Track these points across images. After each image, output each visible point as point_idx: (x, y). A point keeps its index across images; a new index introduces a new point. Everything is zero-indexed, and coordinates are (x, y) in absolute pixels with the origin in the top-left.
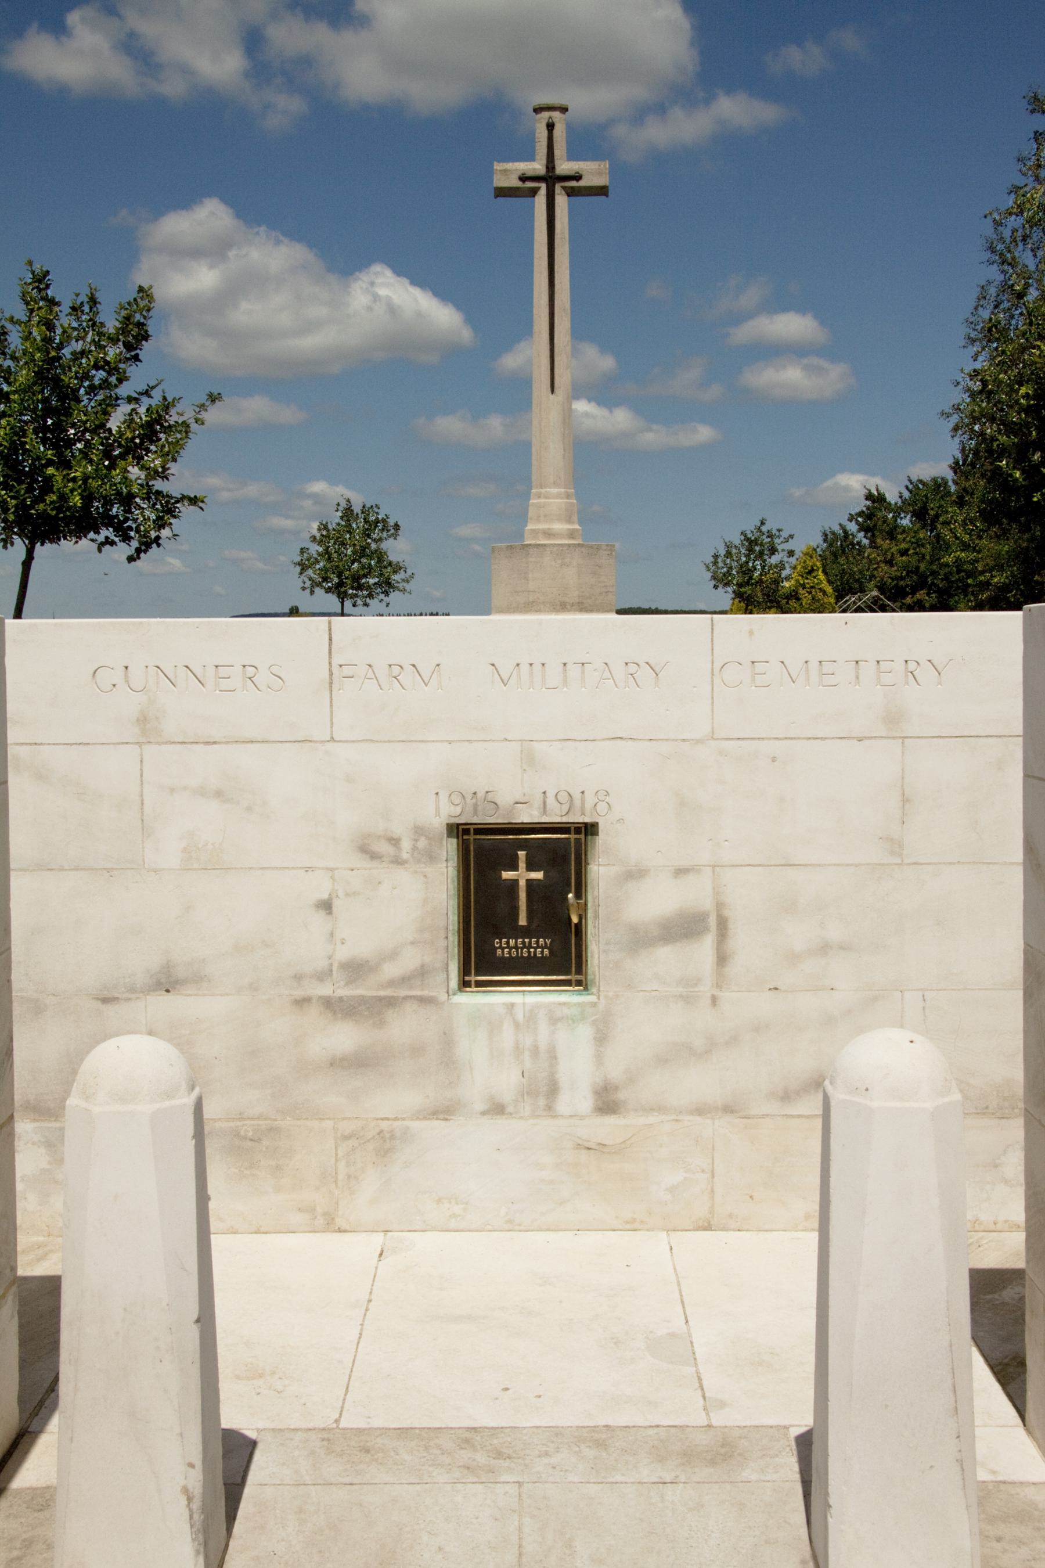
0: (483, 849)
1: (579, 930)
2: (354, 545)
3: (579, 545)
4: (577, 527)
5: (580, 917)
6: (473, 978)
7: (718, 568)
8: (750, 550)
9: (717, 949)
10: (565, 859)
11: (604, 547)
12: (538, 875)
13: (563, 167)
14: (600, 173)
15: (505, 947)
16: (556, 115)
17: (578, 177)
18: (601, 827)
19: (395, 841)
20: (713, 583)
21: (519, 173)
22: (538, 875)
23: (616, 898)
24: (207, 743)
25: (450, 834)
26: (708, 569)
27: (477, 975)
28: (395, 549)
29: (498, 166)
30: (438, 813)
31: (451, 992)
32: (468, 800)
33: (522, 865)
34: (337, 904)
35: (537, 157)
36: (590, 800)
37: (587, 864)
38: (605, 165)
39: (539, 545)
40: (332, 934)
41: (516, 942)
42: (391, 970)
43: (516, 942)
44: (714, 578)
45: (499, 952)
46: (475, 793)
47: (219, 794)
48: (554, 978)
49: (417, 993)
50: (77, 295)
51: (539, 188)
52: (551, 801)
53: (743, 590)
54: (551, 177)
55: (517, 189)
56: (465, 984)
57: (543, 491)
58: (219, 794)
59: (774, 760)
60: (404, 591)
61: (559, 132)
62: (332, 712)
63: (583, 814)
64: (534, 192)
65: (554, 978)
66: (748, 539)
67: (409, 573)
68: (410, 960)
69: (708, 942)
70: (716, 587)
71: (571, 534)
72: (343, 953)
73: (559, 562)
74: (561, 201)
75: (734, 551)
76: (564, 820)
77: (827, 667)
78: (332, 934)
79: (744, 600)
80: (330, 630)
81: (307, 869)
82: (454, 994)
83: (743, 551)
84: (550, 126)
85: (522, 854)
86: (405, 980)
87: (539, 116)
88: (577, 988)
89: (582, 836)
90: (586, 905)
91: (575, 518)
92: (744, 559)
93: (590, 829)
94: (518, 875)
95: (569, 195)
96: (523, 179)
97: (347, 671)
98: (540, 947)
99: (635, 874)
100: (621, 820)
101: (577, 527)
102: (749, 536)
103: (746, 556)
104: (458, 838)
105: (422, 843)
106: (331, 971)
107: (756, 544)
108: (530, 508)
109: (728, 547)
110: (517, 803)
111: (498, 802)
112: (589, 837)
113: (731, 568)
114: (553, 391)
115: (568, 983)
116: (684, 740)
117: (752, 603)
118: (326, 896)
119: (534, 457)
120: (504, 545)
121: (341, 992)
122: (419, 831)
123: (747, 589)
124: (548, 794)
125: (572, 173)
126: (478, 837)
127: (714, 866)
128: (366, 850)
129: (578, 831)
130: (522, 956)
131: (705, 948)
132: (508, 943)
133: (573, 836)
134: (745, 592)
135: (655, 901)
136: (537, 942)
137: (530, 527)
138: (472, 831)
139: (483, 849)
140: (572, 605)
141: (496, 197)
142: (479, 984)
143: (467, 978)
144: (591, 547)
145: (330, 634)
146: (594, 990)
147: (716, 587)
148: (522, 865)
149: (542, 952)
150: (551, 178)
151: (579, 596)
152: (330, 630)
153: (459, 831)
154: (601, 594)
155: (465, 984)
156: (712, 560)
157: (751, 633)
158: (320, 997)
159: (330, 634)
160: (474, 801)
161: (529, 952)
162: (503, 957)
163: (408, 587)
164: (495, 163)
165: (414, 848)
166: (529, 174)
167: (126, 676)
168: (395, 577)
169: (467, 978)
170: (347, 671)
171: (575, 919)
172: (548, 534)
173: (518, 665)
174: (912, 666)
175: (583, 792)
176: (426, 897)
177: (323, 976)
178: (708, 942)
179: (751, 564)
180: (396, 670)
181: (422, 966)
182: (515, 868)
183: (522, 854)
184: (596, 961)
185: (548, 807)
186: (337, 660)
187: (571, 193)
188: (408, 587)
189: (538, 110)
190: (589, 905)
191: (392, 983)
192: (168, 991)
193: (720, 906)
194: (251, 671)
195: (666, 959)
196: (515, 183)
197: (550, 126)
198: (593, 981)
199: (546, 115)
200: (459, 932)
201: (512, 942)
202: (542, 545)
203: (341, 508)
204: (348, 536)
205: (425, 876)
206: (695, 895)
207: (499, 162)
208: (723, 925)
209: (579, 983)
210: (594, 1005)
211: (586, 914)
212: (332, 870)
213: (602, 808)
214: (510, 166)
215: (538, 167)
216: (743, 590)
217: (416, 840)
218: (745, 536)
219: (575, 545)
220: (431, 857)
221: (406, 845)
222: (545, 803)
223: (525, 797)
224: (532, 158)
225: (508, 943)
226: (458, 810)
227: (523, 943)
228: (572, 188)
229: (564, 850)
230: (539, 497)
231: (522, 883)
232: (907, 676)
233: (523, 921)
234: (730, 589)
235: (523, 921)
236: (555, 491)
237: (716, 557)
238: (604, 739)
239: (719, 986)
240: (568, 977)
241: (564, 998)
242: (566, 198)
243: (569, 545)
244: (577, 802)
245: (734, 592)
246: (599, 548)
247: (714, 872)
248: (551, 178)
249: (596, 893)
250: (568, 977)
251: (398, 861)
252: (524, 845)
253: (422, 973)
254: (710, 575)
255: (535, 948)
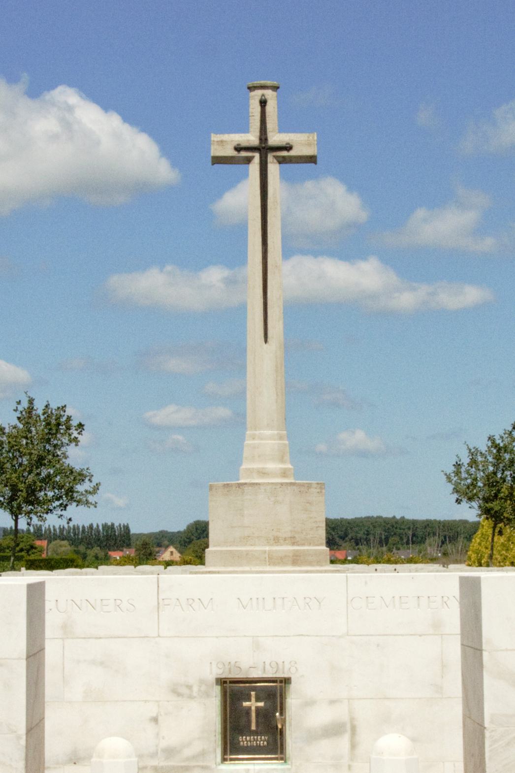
0: (233, 691)
1: (282, 732)
2: (30, 454)
3: (291, 484)
4: (290, 466)
5: (282, 726)
6: (228, 757)
7: (461, 479)
8: (498, 458)
9: (351, 741)
10: (274, 695)
11: (315, 486)
12: (261, 704)
13: (275, 138)
14: (309, 145)
15: (244, 740)
16: (269, 94)
17: (288, 148)
18: (292, 679)
19: (190, 687)
20: (456, 496)
21: (235, 144)
22: (261, 704)
23: (300, 716)
24: (96, 638)
25: (217, 684)
26: (449, 479)
27: (230, 755)
28: (75, 456)
29: (215, 138)
30: (211, 673)
31: (217, 764)
32: (226, 666)
33: (253, 699)
34: (160, 718)
35: (251, 129)
36: (287, 666)
37: (286, 698)
38: (314, 137)
39: (253, 484)
40: (158, 734)
41: (250, 738)
42: (188, 752)
43: (250, 738)
44: (456, 490)
45: (242, 743)
46: (230, 663)
47: (102, 663)
48: (269, 756)
49: (201, 764)
50: (19, 403)
51: (253, 157)
52: (268, 667)
53: (489, 505)
54: (264, 148)
55: (232, 157)
56: (224, 760)
57: (257, 432)
58: (102, 663)
59: (378, 645)
60: (87, 503)
61: (272, 108)
62: (159, 622)
63: (283, 673)
64: (249, 160)
65: (269, 756)
66: (496, 446)
67: (95, 480)
68: (197, 747)
69: (346, 737)
70: (458, 501)
71: (284, 473)
72: (163, 744)
73: (273, 499)
74: (273, 168)
75: (480, 459)
76: (274, 676)
77: (105, 602)
78: (158, 734)
79: (492, 516)
80: (158, 581)
81: (146, 701)
82: (219, 765)
83: (490, 459)
84: (263, 103)
85: (253, 693)
86: (194, 757)
87: (253, 94)
88: (281, 761)
89: (283, 684)
90: (285, 719)
91: (287, 457)
92: (491, 469)
93: (287, 681)
94: (252, 704)
95: (280, 163)
96: (238, 149)
97: (166, 602)
98: (262, 741)
99: (309, 703)
100: (303, 676)
101: (290, 466)
102: (498, 441)
103: (494, 465)
104: (221, 685)
105: (203, 688)
106: (157, 753)
107: (505, 451)
108: (245, 449)
109: (473, 453)
110: (250, 667)
111: (241, 667)
112: (287, 685)
113: (476, 479)
114: (266, 341)
115: (276, 759)
116: (333, 636)
117: (501, 521)
118: (155, 715)
119: (248, 402)
120: (221, 483)
121: (162, 764)
122: (202, 682)
123: (495, 505)
124: (266, 663)
125: (284, 144)
126: (231, 685)
127: (349, 699)
128: (175, 691)
129: (281, 682)
130: (253, 746)
131: (344, 741)
132: (246, 739)
133: (278, 684)
134: (492, 509)
135: (320, 716)
136: (261, 738)
137: (244, 466)
138: (228, 682)
139: (233, 691)
140: (285, 539)
141: (213, 164)
142: (231, 760)
143: (225, 757)
144: (303, 485)
145: (158, 584)
146: (289, 762)
147: (458, 501)
148: (253, 699)
149: (263, 743)
150: (264, 149)
151: (291, 531)
152: (158, 581)
153: (222, 682)
154: (312, 529)
155: (224, 760)
156: (453, 469)
157: (366, 583)
158: (152, 766)
159: (158, 584)
160: (229, 666)
161: (257, 744)
162: (243, 746)
163: (91, 498)
164: (212, 135)
165: (199, 690)
166: (244, 144)
167: (57, 605)
168: (80, 488)
169: (225, 757)
170: (166, 602)
171: (280, 726)
172: (263, 473)
173: (251, 599)
174: (445, 599)
175: (283, 662)
176: (208, 713)
177: (154, 755)
178: (346, 737)
179: (499, 475)
180: (191, 601)
181: (203, 750)
182: (250, 700)
183: (253, 693)
184: (290, 748)
185: (266, 669)
186: (161, 597)
187: (282, 161)
188: (91, 498)
189: (251, 88)
190: (287, 719)
191: (188, 759)
192: (75, 763)
193: (352, 719)
194: (118, 602)
195: (325, 746)
196: (230, 152)
197: (263, 103)
198: (289, 758)
199: (258, 93)
200: (221, 733)
201: (248, 738)
202: (257, 484)
203: (20, 408)
204: (24, 442)
205: (205, 705)
206: (340, 713)
207: (216, 133)
208: (354, 729)
209: (282, 759)
210: (289, 769)
211: (285, 724)
212: (157, 701)
213: (293, 670)
214: (226, 137)
215: (252, 138)
216: (489, 505)
217: (200, 687)
218: (493, 442)
219: (287, 484)
220: (207, 695)
221: (195, 689)
222: (264, 667)
223: (255, 665)
224: (245, 130)
225: (246, 739)
226: (221, 671)
227: (254, 738)
228: (284, 157)
229: (275, 692)
230: (254, 439)
231: (253, 708)
232: (443, 604)
233: (253, 727)
234: (475, 504)
235: (253, 727)
236: (268, 432)
237: (458, 466)
238: (294, 636)
239: (352, 760)
240: (277, 756)
241: (274, 767)
242: (277, 165)
243: (282, 484)
244: (281, 667)
245: (480, 507)
246: (309, 486)
247: (349, 702)
248: (264, 149)
249: (290, 713)
250: (277, 756)
251: (191, 697)
252: (254, 689)
253: (203, 754)
254: (451, 487)
255: (260, 742)
